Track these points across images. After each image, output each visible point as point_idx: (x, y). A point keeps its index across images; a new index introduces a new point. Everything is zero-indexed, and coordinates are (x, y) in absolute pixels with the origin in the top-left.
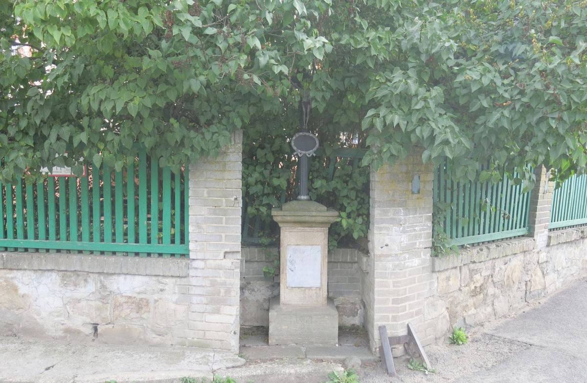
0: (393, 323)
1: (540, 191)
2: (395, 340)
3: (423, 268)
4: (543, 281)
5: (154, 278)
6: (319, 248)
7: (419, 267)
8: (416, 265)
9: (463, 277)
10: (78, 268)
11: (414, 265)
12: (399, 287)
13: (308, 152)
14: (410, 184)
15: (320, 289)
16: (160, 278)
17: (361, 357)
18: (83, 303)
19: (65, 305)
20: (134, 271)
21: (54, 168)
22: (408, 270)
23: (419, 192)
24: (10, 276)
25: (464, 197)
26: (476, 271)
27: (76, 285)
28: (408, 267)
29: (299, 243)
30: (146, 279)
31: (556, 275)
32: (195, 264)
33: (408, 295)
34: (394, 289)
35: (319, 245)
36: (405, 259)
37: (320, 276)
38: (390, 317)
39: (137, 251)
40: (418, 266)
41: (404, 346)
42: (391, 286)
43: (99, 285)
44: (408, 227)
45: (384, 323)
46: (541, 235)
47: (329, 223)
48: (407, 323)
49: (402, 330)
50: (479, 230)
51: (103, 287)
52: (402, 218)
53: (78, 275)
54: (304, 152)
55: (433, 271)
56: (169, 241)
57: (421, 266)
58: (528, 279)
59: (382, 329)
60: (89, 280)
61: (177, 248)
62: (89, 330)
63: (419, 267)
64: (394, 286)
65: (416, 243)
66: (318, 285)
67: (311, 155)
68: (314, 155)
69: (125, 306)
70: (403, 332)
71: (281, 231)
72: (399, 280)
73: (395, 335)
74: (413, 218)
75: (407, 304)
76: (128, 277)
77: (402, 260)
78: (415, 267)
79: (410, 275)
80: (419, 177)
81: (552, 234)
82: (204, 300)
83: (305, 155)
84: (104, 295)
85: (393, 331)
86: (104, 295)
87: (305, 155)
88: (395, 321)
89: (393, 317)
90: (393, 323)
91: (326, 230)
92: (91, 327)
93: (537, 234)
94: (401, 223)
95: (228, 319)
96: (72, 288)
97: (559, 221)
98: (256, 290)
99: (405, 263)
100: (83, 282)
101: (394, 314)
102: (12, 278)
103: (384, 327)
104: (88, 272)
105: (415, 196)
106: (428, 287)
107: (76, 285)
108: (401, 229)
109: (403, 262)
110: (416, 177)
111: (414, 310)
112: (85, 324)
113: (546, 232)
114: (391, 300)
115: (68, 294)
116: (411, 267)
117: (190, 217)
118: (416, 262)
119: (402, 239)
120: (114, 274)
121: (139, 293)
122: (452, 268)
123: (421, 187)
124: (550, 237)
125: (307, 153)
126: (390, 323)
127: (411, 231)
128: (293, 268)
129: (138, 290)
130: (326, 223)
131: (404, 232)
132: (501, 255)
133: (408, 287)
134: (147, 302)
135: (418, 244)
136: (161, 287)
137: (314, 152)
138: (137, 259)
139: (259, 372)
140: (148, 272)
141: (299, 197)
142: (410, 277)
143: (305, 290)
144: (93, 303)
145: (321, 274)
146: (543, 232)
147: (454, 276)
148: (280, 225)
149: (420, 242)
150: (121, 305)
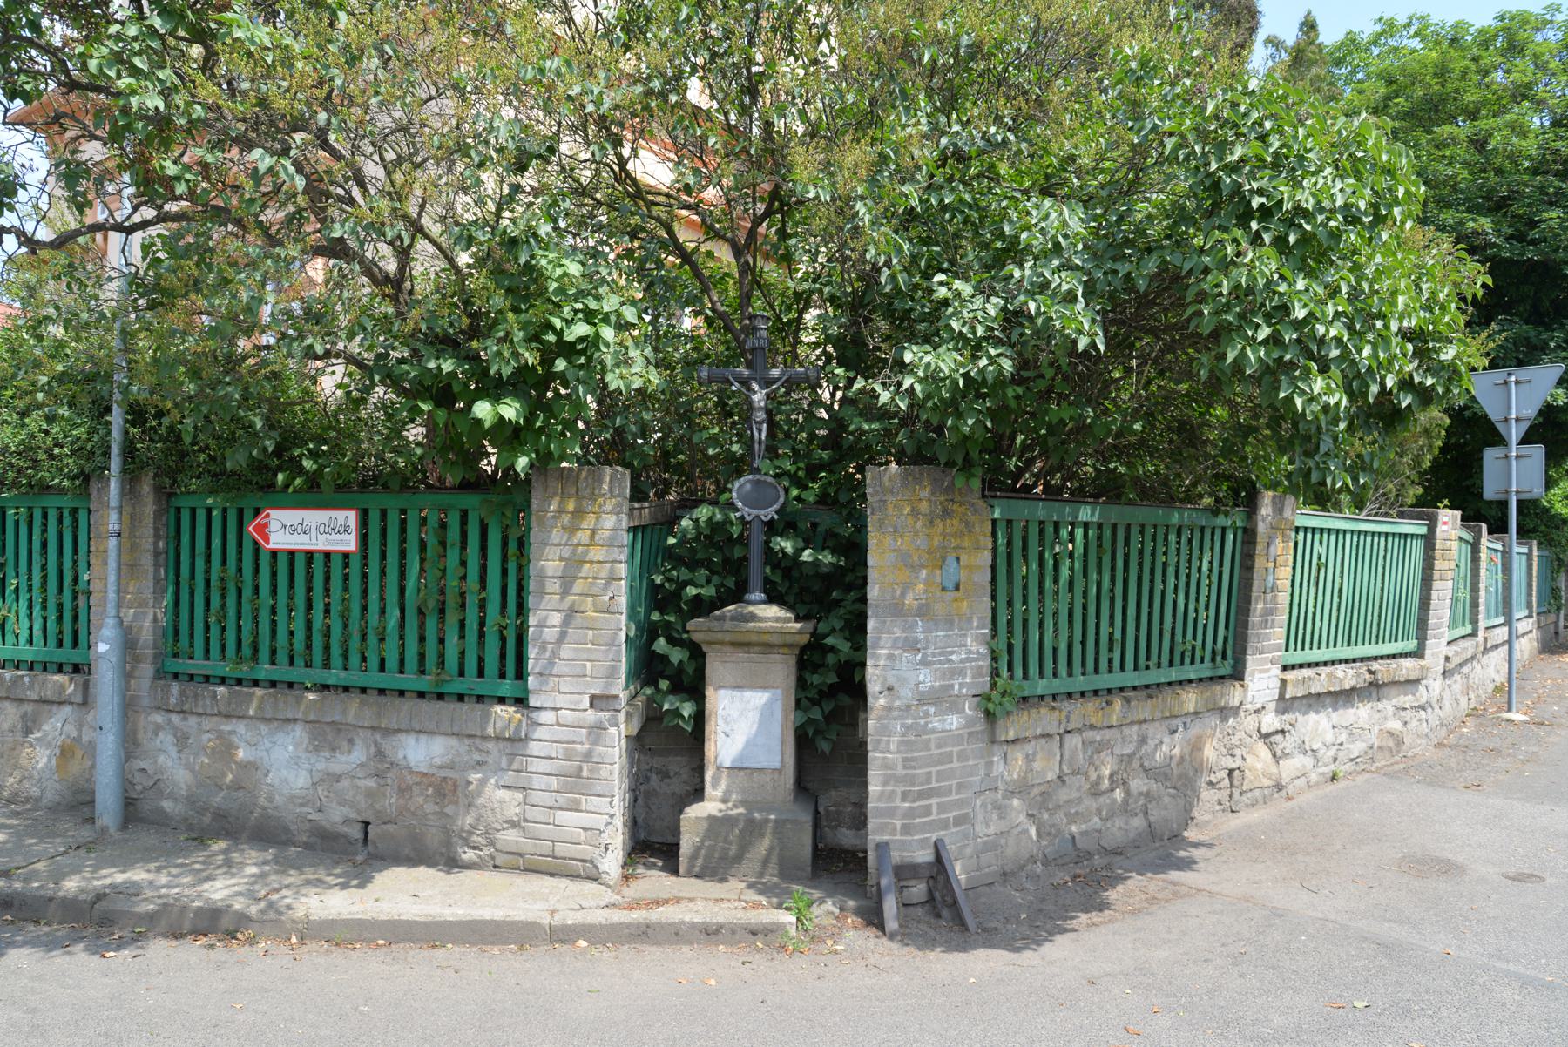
1: (1255, 588)
2: (905, 872)
3: (970, 734)
4: (1274, 769)
5: (467, 741)
9: (1066, 756)
10: (337, 718)
14: (938, 572)
15: (779, 771)
16: (478, 741)
18: (345, 783)
19: (314, 784)
20: (433, 727)
23: (957, 588)
24: (226, 728)
25: (1176, 587)
26: (1100, 747)
27: (333, 750)
28: (933, 731)
30: (453, 742)
31: (1308, 761)
32: (546, 717)
33: (934, 784)
36: (927, 714)
39: (381, 686)
43: (373, 750)
44: (934, 655)
46: (1261, 681)
50: (1083, 664)
51: (380, 754)
52: (921, 636)
53: (339, 730)
54: (755, 512)
55: (993, 742)
56: (496, 672)
58: (1234, 766)
59: (883, 847)
60: (358, 742)
61: (507, 687)
62: (356, 832)
64: (905, 767)
65: (952, 686)
66: (777, 765)
69: (416, 790)
70: (924, 856)
73: (907, 860)
75: (934, 801)
76: (423, 737)
79: (939, 746)
80: (958, 559)
81: (1290, 675)
82: (554, 782)
84: (382, 765)
86: (382, 765)
89: (904, 826)
91: (792, 661)
92: (359, 826)
93: (1252, 675)
95: (604, 820)
96: (327, 754)
97: (1315, 650)
100: (345, 743)
102: (230, 733)
104: (355, 726)
105: (949, 596)
106: (982, 772)
107: (333, 750)
110: (951, 560)
111: (951, 815)
112: (346, 821)
113: (1276, 670)
115: (321, 766)
118: (954, 722)
119: (921, 678)
120: (399, 731)
121: (441, 767)
122: (1043, 736)
123: (963, 579)
124: (1283, 682)
125: (762, 512)
127: (940, 662)
128: (727, 730)
129: (438, 761)
130: (790, 646)
131: (925, 663)
132: (1158, 715)
134: (455, 786)
136: (477, 757)
138: (440, 704)
139: (110, 674)
140: (456, 730)
141: (747, 597)
144: (362, 783)
146: (1268, 671)
147: (1036, 755)
148: (705, 649)
150: (409, 788)
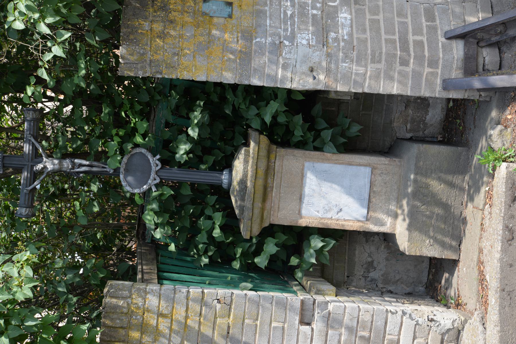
0: (440, 67)
6: (307, 164)
7: (353, 11)
8: (349, 17)
11: (349, 22)
12: (381, 53)
13: (153, 168)
14: (215, 20)
15: (373, 169)
17: (489, 129)
21: (138, 338)
22: (355, 36)
23: (230, 4)
28: (351, 35)
29: (298, 196)
33: (397, 37)
34: (383, 62)
35: (304, 166)
36: (336, 40)
37: (354, 167)
38: (431, 70)
40: (351, 14)
41: (482, 47)
42: (378, 66)
44: (286, 30)
45: (439, 81)
47: (269, 146)
48: (444, 40)
49: (455, 52)
54: (153, 175)
57: (353, 5)
59: (447, 85)
63: (353, 11)
64: (379, 62)
65: (314, 15)
66: (368, 170)
67: (158, 162)
68: (158, 157)
70: (458, 49)
71: (277, 223)
72: (369, 51)
73: (460, 64)
74: (271, 19)
75: (411, 38)
77: (339, 44)
78: (351, 20)
79: (364, 31)
83: (157, 172)
85: (455, 66)
87: (157, 172)
88: (437, 62)
89: (430, 65)
90: (440, 67)
91: (282, 151)
94: (277, 42)
98: (370, 259)
99: (344, 40)
101: (426, 64)
103: (444, 81)
105: (236, 12)
108: (287, 43)
109: (342, 44)
111: (425, 24)
114: (402, 68)
116: (352, 27)
117: (265, 85)
119: (304, 42)
125: (154, 169)
126: (439, 71)
127: (293, 25)
128: (336, 210)
130: (269, 152)
131: (292, 38)
133: (384, 36)
135: (315, 12)
137: (154, 156)
141: (225, 186)
142: (368, 31)
143: (374, 192)
145: (351, 165)
148: (266, 224)
149: (312, 9)
